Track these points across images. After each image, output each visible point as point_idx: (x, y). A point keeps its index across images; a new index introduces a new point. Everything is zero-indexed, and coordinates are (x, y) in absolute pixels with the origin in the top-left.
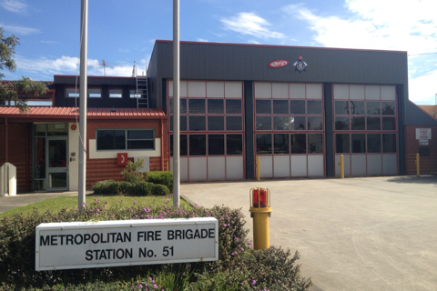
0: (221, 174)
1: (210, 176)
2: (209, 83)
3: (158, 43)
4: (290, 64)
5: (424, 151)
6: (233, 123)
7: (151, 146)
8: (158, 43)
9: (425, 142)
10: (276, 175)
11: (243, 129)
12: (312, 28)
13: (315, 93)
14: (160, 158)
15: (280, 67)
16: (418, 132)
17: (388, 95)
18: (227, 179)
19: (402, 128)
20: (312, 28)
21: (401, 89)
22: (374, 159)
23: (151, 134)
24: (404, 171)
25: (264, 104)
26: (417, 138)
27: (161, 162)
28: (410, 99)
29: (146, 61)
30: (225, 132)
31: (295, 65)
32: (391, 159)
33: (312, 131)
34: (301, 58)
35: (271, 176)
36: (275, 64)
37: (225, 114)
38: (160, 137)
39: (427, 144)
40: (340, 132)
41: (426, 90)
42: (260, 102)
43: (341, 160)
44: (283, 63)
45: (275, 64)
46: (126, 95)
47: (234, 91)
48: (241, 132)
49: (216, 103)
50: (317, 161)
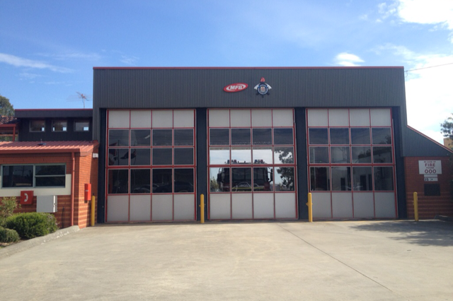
0: (167, 215)
1: (177, 216)
2: (155, 113)
3: (98, 72)
4: (250, 87)
5: (430, 189)
6: (183, 155)
7: (61, 183)
8: (98, 72)
9: (433, 178)
10: (234, 217)
11: (195, 163)
12: (443, 25)
13: (284, 119)
14: (70, 196)
15: (237, 92)
16: (423, 166)
17: (382, 119)
18: (174, 221)
19: (400, 160)
20: (443, 25)
21: (398, 113)
22: (363, 199)
23: (61, 170)
24: (402, 216)
25: (320, 133)
26: (422, 171)
27: (70, 201)
28: (408, 124)
29: (89, 92)
30: (173, 165)
31: (256, 88)
32: (386, 199)
33: (278, 161)
34: (263, 80)
35: (229, 217)
36: (233, 88)
37: (173, 146)
38: (71, 173)
39: (436, 180)
40: (116, 167)
41: (425, 116)
42: (314, 130)
43: (315, 199)
44: (241, 87)
45: (233, 88)
46: (70, 127)
47: (186, 120)
48: (193, 165)
49: (162, 135)
50: (287, 201)
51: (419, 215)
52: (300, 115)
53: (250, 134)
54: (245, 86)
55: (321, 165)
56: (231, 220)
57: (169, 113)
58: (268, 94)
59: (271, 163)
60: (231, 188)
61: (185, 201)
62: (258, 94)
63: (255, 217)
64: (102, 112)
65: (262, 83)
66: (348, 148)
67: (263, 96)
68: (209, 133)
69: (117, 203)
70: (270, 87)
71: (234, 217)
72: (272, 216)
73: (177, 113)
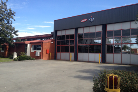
15: (84, 22)
31: (90, 20)
34: (92, 17)
40: (80, 45)
44: (85, 20)
49: (68, 36)
51: (51, 59)
52: (104, 27)
53: (88, 34)
54: (86, 20)
55: (92, 44)
56: (83, 61)
57: (129, 23)
58: (93, 21)
59: (113, 43)
60: (95, 52)
61: (72, 55)
62: (90, 22)
63: (89, 61)
64: (56, 31)
65: (92, 18)
66: (84, 38)
67: (91, 22)
68: (106, 33)
69: (58, 54)
70: (94, 19)
71: (84, 60)
72: (94, 61)
73: (62, 31)
